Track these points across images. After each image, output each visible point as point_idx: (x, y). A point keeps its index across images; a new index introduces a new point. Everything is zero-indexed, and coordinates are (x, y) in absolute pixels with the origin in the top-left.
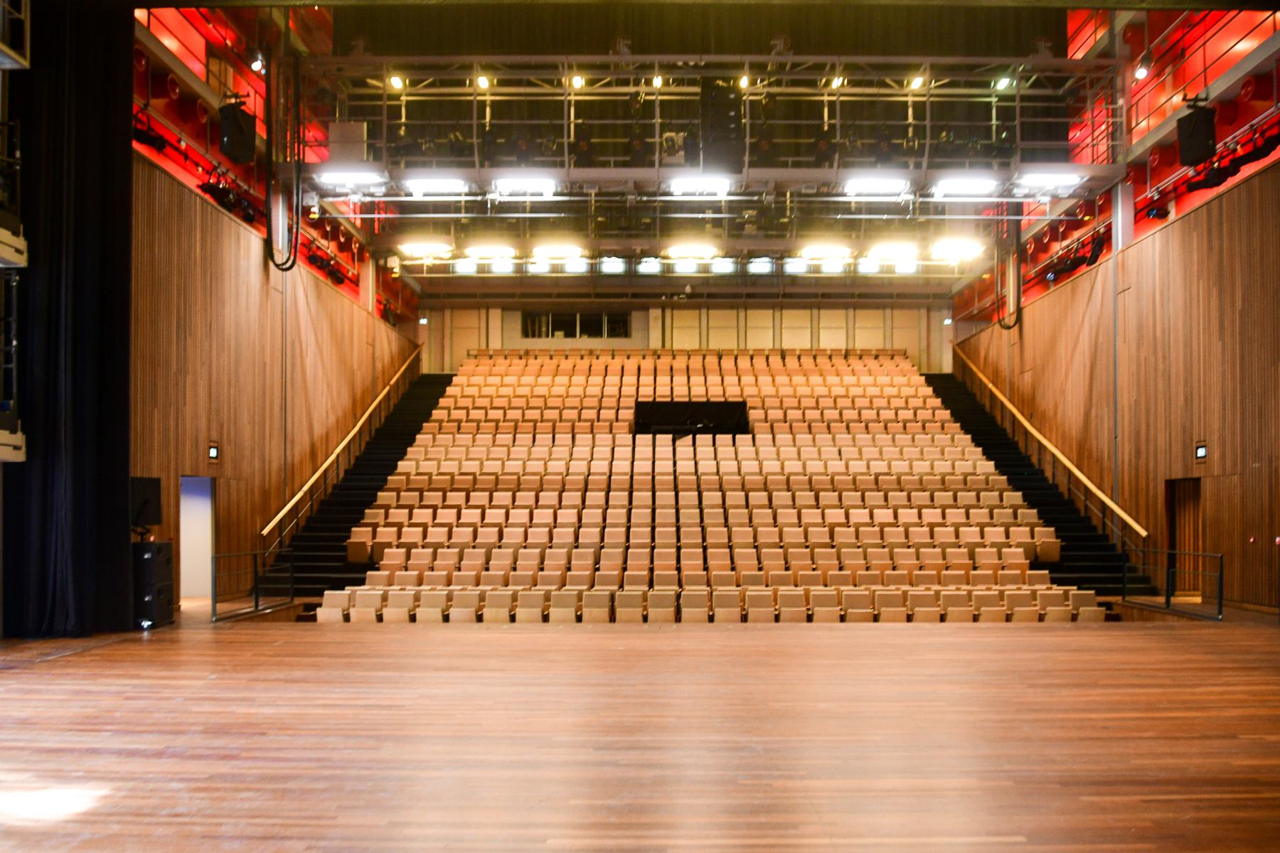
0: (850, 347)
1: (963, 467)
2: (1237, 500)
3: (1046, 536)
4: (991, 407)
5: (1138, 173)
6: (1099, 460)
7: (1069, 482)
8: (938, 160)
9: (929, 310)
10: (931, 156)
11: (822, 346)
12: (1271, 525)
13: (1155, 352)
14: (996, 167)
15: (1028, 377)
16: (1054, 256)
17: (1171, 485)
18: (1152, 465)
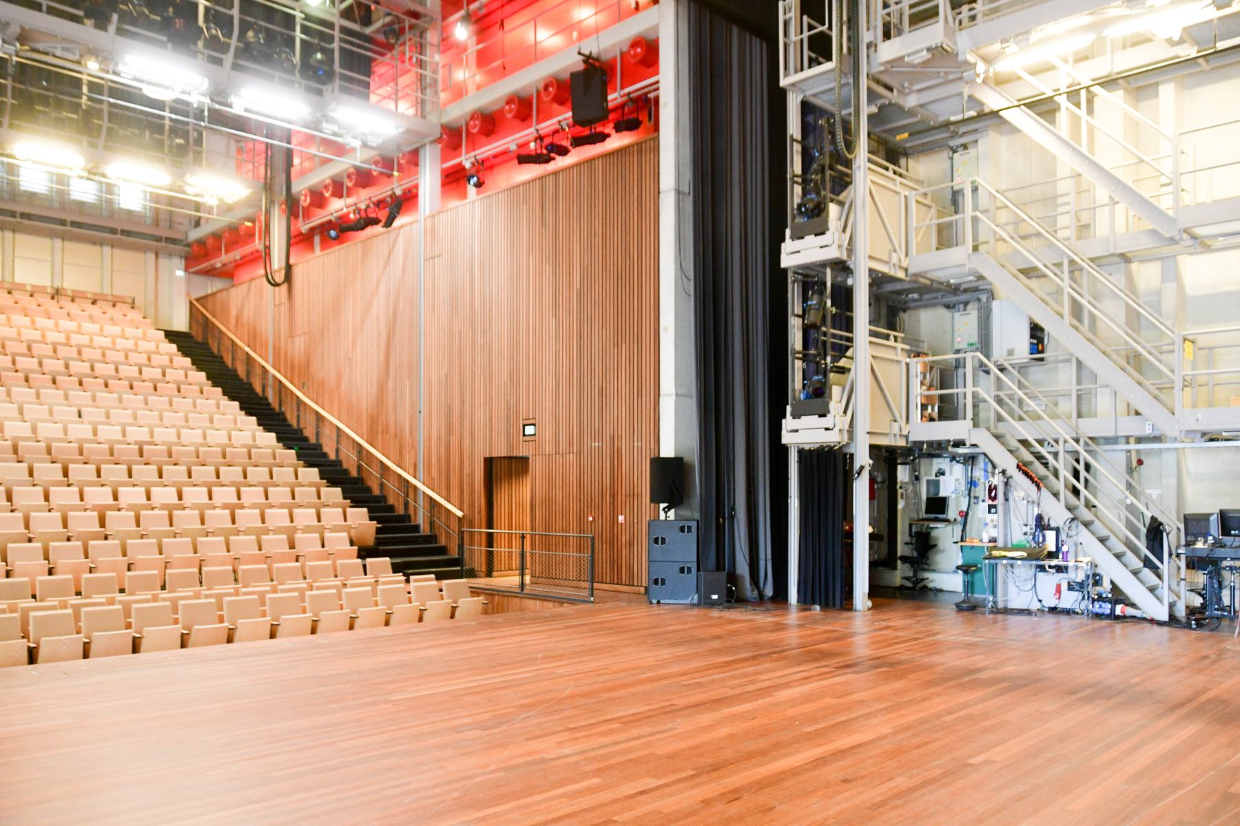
0: (57, 284)
1: (218, 437)
2: (573, 479)
3: (360, 517)
4: (248, 373)
5: (452, 138)
6: (398, 437)
7: (360, 459)
8: (242, 62)
9: (157, 255)
10: (236, 56)
11: (18, 280)
12: (613, 503)
13: (473, 326)
14: (85, 143)
15: (299, 343)
16: (347, 213)
17: (489, 462)
18: (467, 441)
